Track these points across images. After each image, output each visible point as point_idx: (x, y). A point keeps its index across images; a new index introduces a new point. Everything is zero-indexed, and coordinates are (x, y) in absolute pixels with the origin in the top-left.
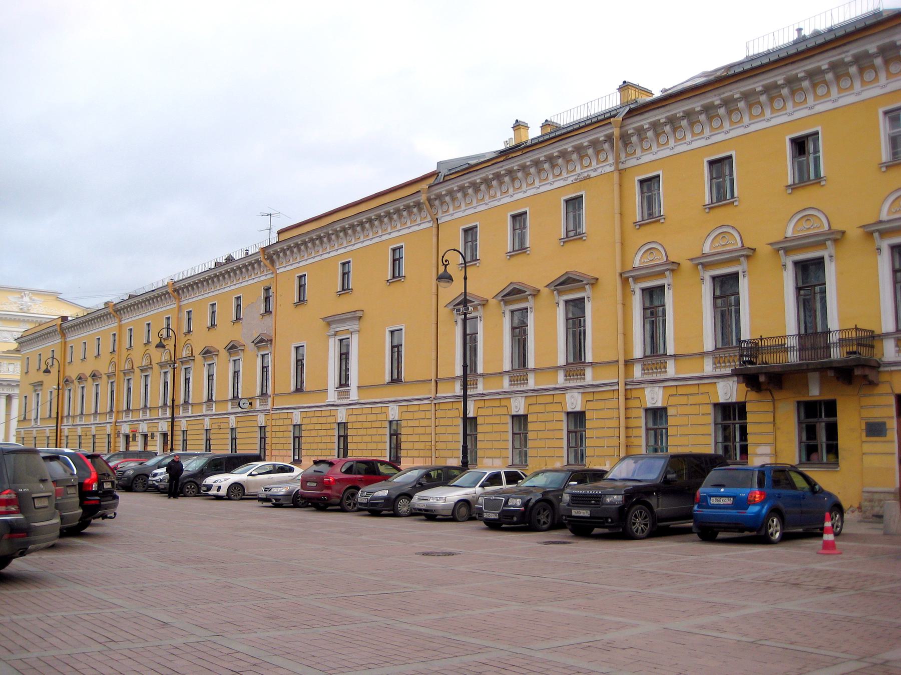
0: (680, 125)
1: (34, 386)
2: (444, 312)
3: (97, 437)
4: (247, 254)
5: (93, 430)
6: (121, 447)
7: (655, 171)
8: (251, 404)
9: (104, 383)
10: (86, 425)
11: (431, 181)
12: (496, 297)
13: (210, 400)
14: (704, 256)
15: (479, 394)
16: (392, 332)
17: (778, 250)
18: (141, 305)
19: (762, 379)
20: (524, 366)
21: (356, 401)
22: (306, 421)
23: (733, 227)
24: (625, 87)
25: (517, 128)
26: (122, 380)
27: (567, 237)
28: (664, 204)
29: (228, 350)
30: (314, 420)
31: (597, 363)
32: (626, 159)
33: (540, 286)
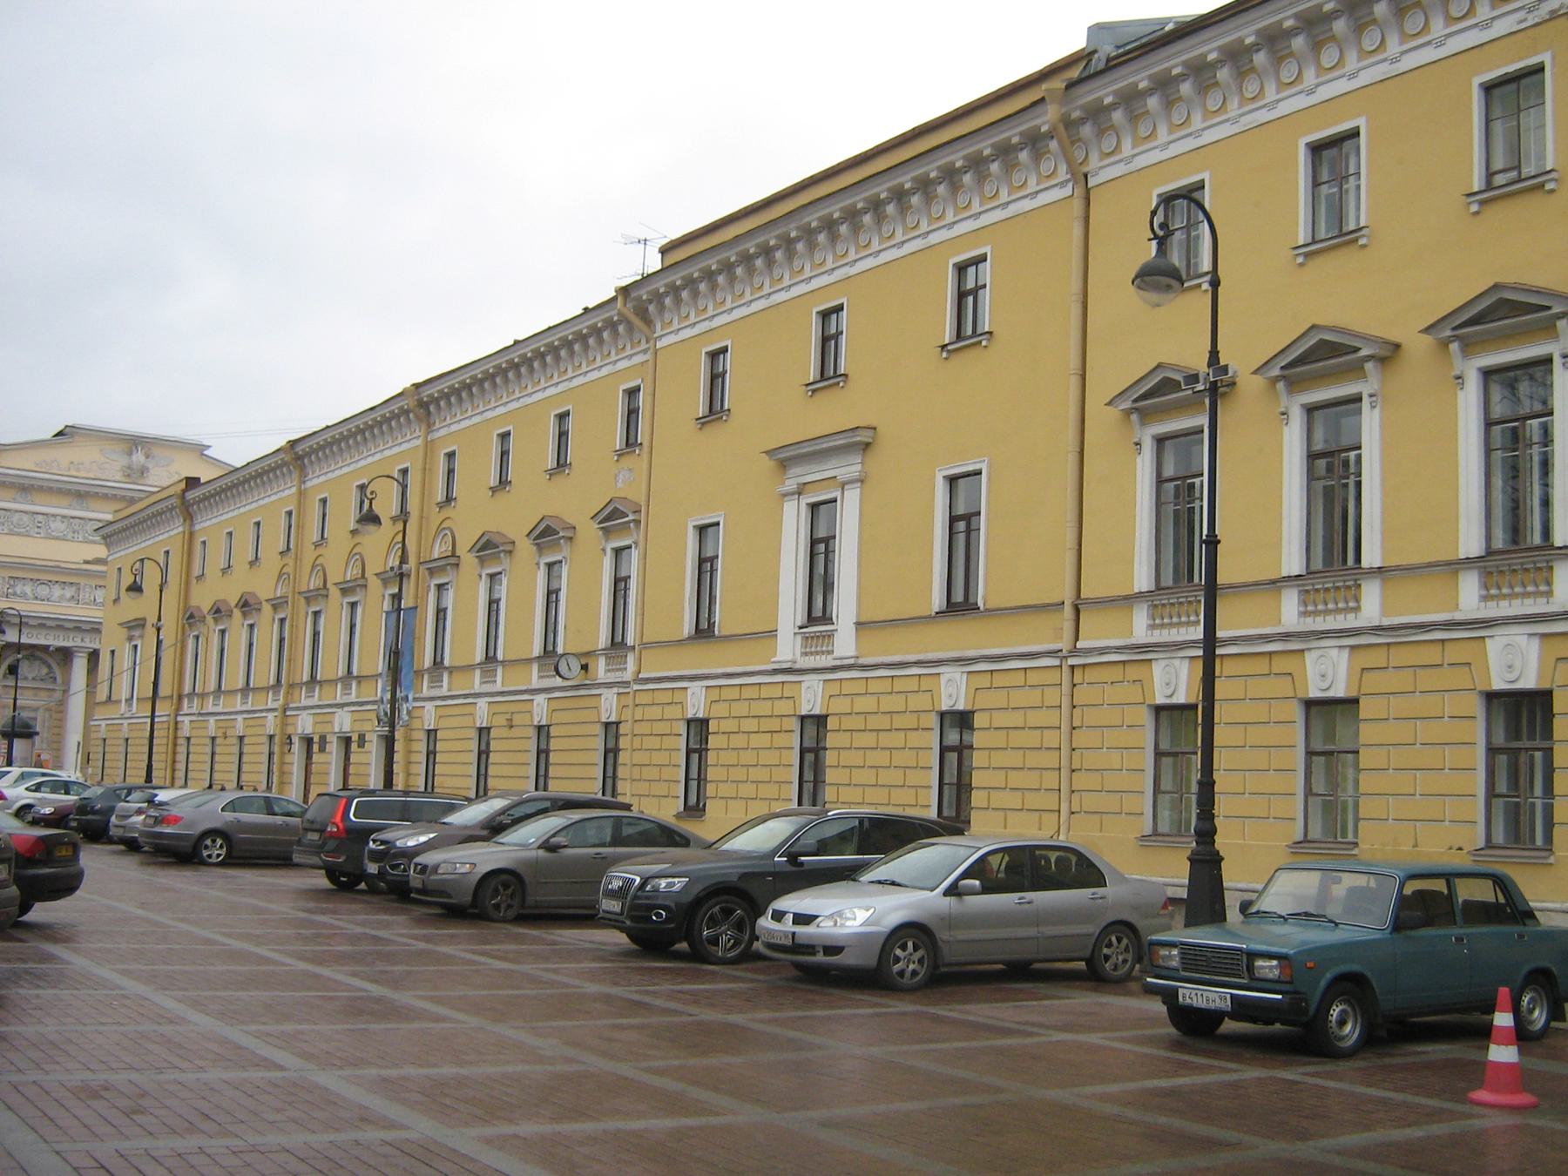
0: (1145, 110)
1: (130, 628)
2: (1103, 419)
3: (246, 740)
6: (296, 765)
8: (585, 667)
9: (266, 622)
10: (225, 714)
11: (1075, 73)
12: (1265, 369)
13: (490, 658)
16: (952, 481)
17: (1445, 344)
18: (372, 432)
21: (852, 661)
22: (558, 718)
26: (302, 613)
27: (1489, 186)
30: (740, 709)
31: (1398, 568)
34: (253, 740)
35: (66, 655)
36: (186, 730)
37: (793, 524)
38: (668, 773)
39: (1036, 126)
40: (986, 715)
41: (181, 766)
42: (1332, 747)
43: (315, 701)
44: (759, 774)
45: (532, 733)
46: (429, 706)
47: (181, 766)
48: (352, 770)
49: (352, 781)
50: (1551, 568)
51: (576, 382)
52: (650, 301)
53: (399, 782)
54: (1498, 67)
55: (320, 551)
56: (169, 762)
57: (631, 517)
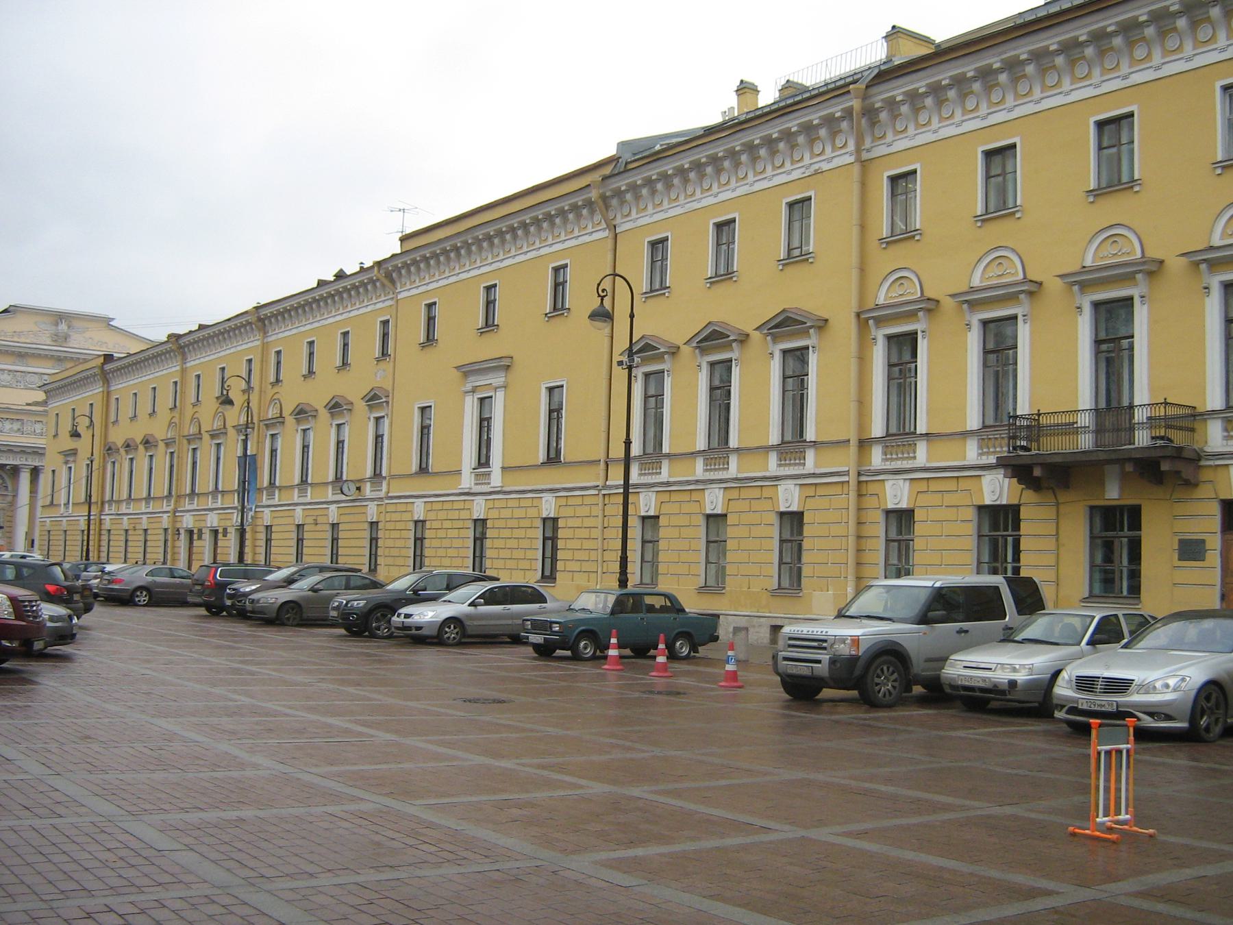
1: (66, 455)
3: (149, 532)
4: (361, 268)
5: (64, 526)
7: (729, 213)
8: (358, 489)
11: (607, 171)
13: (304, 481)
14: (973, 290)
15: (662, 483)
19: (1037, 472)
20: (801, 435)
21: (499, 489)
23: (1111, 226)
24: (895, 34)
25: (741, 92)
27: (789, 256)
28: (1024, 189)
29: (367, 402)
30: (442, 515)
31: (822, 443)
32: (873, 145)
33: (749, 329)
34: (116, 532)
35: (15, 471)
36: (107, 525)
37: (470, 407)
38: (404, 552)
39: (788, 128)
40: (564, 520)
41: (104, 549)
42: (717, 539)
43: (195, 507)
44: (451, 552)
45: (328, 528)
46: (267, 510)
47: (104, 549)
48: (219, 551)
49: (219, 558)
50: (916, 444)
51: (352, 314)
52: (394, 271)
53: (248, 558)
54: (791, 196)
55: (196, 409)
56: (96, 546)
57: (384, 400)
